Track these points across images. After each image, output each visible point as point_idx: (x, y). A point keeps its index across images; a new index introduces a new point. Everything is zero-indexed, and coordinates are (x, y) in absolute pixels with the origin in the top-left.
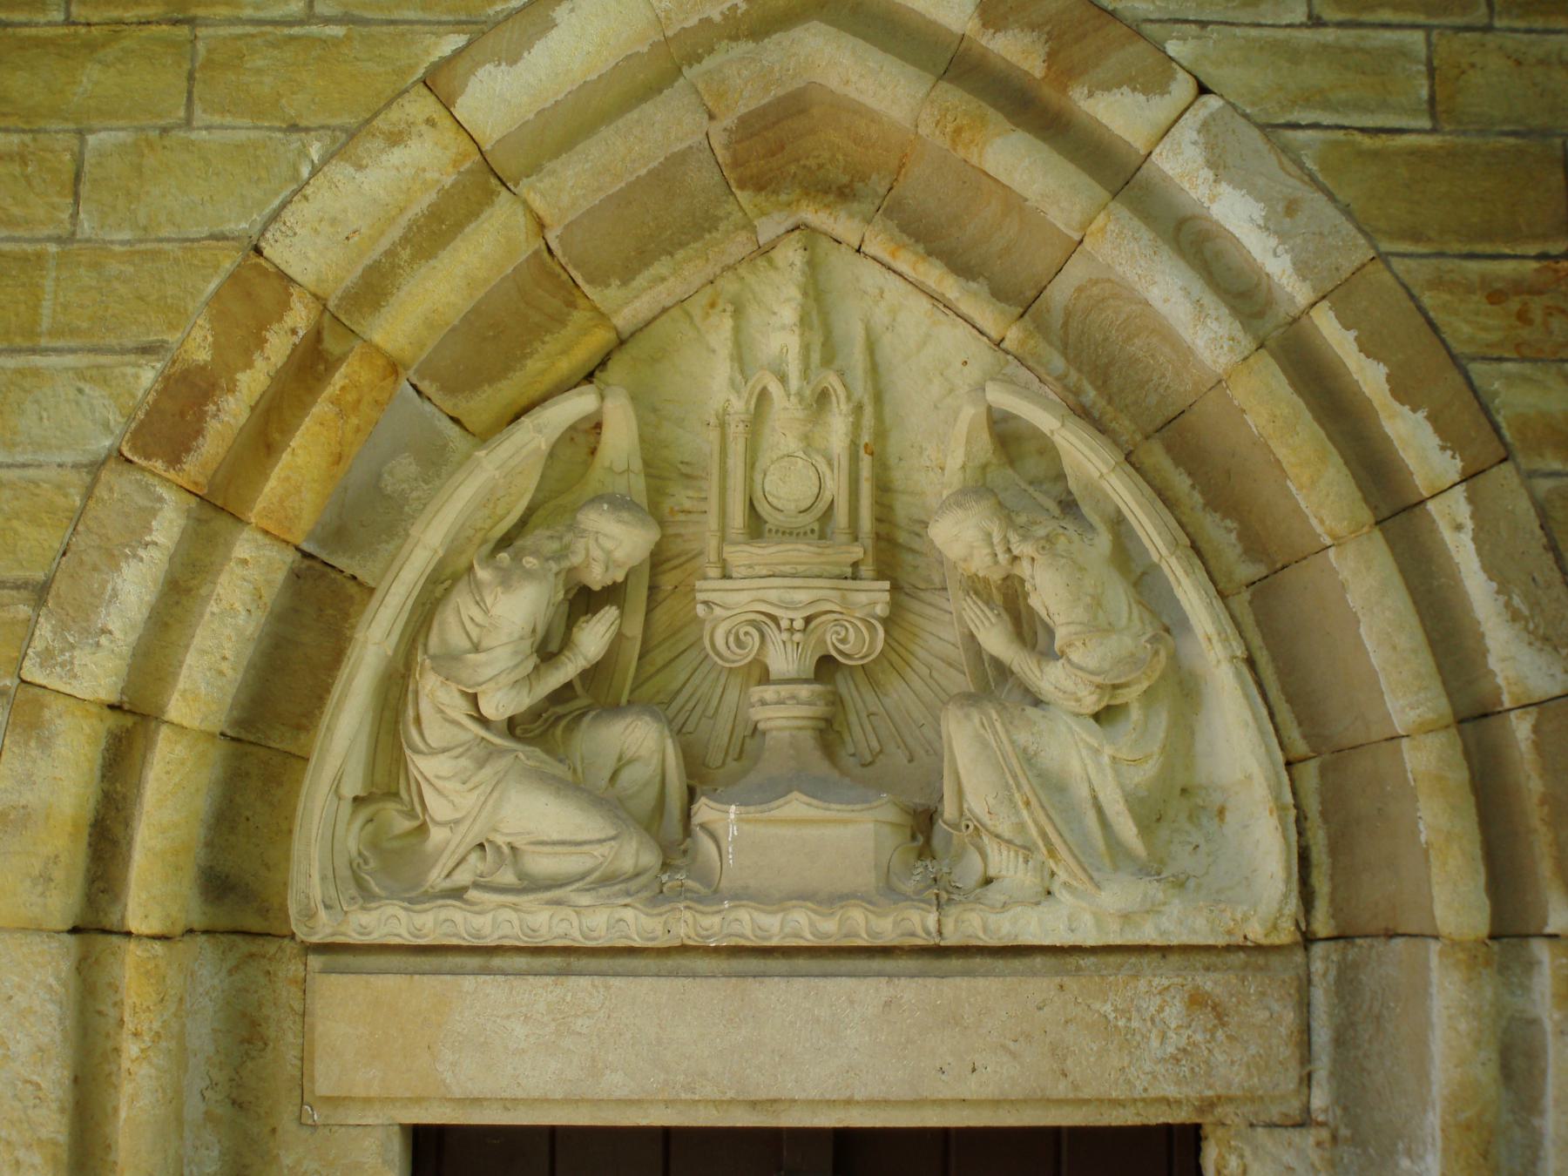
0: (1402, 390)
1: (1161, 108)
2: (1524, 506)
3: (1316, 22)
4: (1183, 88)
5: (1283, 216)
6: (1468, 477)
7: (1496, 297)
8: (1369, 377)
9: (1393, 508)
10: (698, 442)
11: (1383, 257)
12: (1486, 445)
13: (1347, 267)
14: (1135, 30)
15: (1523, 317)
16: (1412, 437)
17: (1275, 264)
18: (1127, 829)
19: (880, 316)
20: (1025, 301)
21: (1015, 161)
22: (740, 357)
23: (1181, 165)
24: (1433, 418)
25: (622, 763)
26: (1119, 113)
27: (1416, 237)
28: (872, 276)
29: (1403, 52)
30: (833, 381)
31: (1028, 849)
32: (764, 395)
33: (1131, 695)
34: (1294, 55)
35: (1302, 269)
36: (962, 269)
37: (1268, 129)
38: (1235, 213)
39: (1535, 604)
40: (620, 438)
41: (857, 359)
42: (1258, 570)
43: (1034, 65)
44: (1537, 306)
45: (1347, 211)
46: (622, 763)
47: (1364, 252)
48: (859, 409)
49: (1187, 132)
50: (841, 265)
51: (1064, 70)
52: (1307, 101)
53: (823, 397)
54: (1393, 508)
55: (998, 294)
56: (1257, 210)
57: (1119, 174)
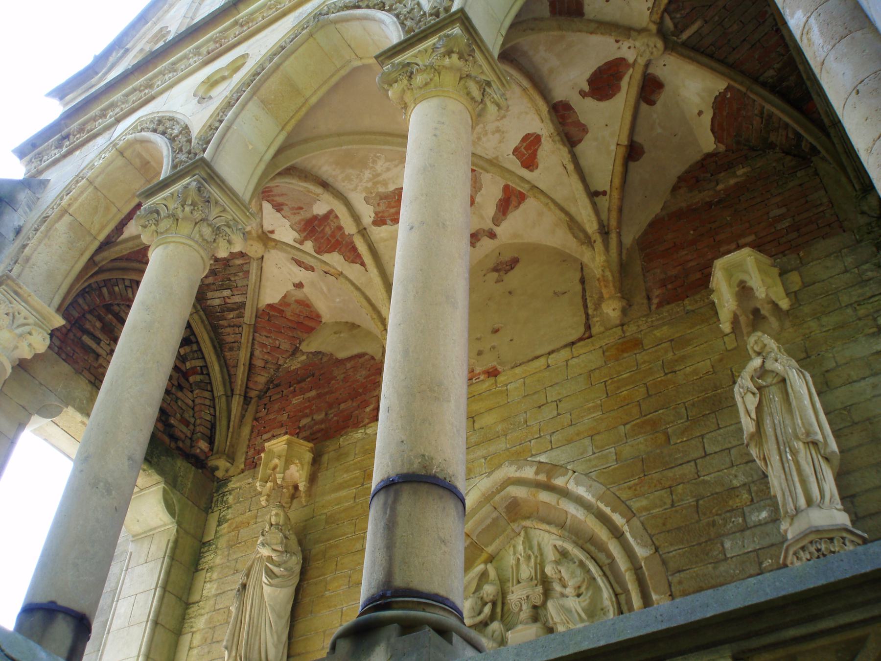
0: (613, 511)
1: (567, 478)
2: (638, 523)
3: (594, 453)
4: (570, 472)
5: (589, 488)
6: (627, 522)
7: (630, 488)
8: (607, 510)
9: (617, 534)
10: (509, 573)
11: (608, 489)
12: (630, 514)
13: (601, 493)
14: (562, 466)
15: (635, 490)
16: (618, 519)
17: (588, 497)
18: (583, 615)
19: (540, 539)
20: (562, 526)
21: (545, 497)
22: (515, 554)
23: (572, 487)
24: (620, 514)
25: (494, 632)
26: (559, 482)
27: (614, 483)
28: (538, 532)
29: (610, 453)
30: (530, 552)
31: (564, 623)
32: (518, 559)
33: (583, 589)
34: (590, 460)
35: (593, 496)
36: (549, 523)
37: (586, 475)
38: (581, 491)
39: (642, 540)
40: (492, 573)
41: (536, 548)
42: (609, 561)
43: (545, 479)
44: (638, 488)
45: (601, 483)
46: (494, 632)
47: (604, 489)
48: (536, 557)
49: (572, 480)
50: (532, 532)
51: (549, 477)
52: (593, 467)
53: (529, 557)
54: (617, 534)
55: (557, 526)
56: (585, 489)
57: (564, 493)
